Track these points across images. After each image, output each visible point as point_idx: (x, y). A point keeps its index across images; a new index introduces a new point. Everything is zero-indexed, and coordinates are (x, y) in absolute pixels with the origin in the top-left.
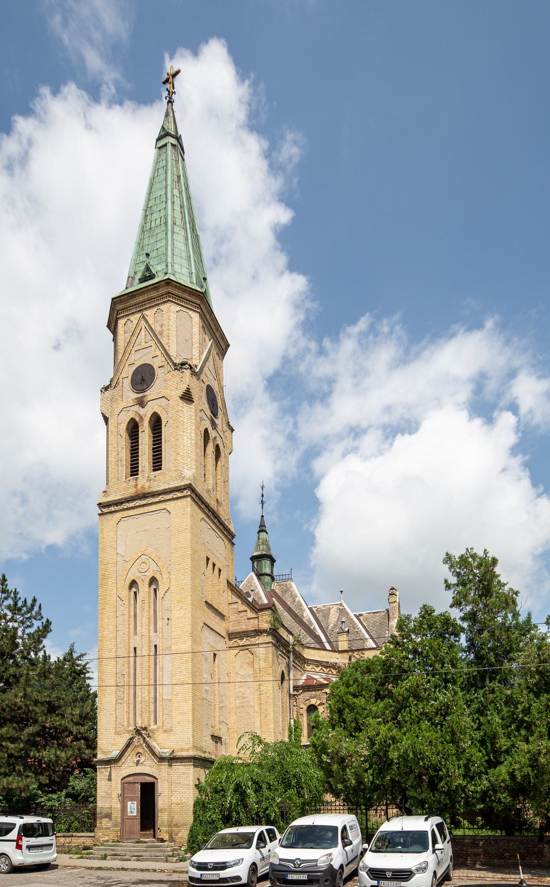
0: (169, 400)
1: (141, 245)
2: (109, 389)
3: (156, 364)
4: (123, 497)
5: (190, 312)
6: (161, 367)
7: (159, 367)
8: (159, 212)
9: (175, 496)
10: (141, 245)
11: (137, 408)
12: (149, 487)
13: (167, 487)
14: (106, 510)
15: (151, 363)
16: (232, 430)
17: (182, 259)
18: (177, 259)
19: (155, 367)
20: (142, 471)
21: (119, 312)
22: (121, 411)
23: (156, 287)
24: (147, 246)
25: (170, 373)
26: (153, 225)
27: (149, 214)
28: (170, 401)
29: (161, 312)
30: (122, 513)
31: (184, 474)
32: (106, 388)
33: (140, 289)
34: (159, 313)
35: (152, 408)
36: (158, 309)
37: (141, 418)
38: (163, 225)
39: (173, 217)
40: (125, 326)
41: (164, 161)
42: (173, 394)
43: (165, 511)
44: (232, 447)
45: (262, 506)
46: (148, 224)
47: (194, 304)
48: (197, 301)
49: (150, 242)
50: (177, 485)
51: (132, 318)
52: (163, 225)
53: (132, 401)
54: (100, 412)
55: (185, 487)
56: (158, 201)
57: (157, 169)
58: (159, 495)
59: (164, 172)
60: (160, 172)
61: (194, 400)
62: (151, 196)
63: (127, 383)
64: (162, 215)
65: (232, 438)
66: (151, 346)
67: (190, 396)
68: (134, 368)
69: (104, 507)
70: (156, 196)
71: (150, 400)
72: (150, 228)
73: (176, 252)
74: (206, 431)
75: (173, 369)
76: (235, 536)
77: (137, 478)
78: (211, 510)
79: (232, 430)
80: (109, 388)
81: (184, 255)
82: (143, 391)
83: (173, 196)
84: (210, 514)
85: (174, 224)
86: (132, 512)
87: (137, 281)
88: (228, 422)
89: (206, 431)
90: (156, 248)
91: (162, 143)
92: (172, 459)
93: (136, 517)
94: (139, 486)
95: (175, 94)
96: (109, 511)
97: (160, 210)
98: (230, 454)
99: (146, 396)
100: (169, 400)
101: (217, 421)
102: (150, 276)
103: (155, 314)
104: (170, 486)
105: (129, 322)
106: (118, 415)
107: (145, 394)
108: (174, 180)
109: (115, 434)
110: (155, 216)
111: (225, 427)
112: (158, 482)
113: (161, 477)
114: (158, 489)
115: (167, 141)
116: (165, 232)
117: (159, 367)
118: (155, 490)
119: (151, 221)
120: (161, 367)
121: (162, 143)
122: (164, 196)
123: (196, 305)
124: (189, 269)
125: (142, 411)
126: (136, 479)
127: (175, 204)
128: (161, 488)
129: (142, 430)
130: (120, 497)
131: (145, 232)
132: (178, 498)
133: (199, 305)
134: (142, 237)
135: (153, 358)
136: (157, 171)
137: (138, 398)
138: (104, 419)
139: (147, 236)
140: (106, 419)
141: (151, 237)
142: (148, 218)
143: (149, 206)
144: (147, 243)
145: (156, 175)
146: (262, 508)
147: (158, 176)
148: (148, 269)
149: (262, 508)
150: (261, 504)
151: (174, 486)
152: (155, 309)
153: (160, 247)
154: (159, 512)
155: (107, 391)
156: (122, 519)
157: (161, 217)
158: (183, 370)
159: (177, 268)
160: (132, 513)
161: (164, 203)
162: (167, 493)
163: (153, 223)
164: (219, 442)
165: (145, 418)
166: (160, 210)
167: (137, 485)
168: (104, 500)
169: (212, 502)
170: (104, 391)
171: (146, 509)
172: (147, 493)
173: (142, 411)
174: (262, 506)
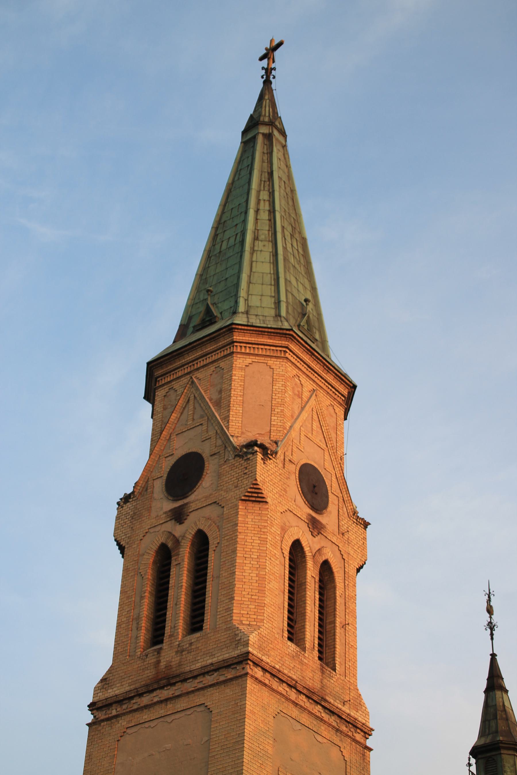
0: (223, 507)
1: (204, 277)
2: (130, 500)
3: (205, 450)
4: (132, 687)
5: (271, 362)
6: (215, 454)
7: (211, 456)
8: (234, 228)
9: (222, 678)
10: (204, 277)
11: (170, 526)
12: (180, 665)
13: (210, 661)
14: (102, 715)
15: (200, 451)
16: (366, 525)
17: (264, 286)
18: (256, 289)
19: (206, 455)
20: (171, 636)
21: (158, 379)
22: (146, 533)
23: (214, 338)
24: (212, 278)
25: (227, 462)
26: (224, 246)
27: (221, 231)
28: (225, 509)
29: (222, 371)
30: (128, 717)
31: (240, 635)
32: (126, 499)
33: (190, 344)
34: (217, 373)
35: (195, 523)
36: (216, 368)
37: (177, 542)
38: (237, 246)
39: (256, 231)
40: (166, 399)
41: (250, 158)
42: (230, 497)
43: (202, 708)
44: (364, 555)
45: (492, 635)
46: (218, 247)
47: (278, 348)
48: (283, 342)
49: (217, 271)
50: (227, 656)
51: (176, 385)
52: (237, 246)
53: (164, 515)
54: (113, 538)
55: (240, 660)
56: (235, 212)
57: (239, 170)
58: (195, 677)
59: (248, 172)
60: (243, 173)
61: (268, 500)
62: (226, 207)
63: (159, 486)
64: (239, 231)
65: (365, 539)
66: (202, 424)
67: (260, 495)
68: (172, 461)
69: (99, 709)
70: (233, 206)
71: (193, 511)
72: (218, 251)
73: (256, 278)
74: (297, 546)
75: (233, 456)
76: (372, 730)
77: (161, 649)
78: (305, 691)
79: (366, 525)
80: (130, 498)
81: (268, 279)
82: (184, 496)
83: (258, 201)
84: (302, 700)
85: (256, 238)
86: (145, 716)
87: (191, 329)
88: (355, 513)
89: (297, 546)
90: (224, 278)
91: (249, 136)
92: (221, 609)
93: (152, 724)
94: (163, 664)
95: (275, 70)
96: (107, 716)
97: (236, 225)
98: (358, 571)
99: (186, 504)
100: (223, 507)
101: (323, 519)
102: (210, 320)
103: (211, 375)
104: (215, 660)
105: (172, 392)
106: (141, 540)
107: (185, 501)
108: (263, 179)
109: (133, 574)
110: (228, 234)
111: (346, 523)
112: (195, 653)
113: (200, 645)
114: (193, 667)
115: (257, 132)
116: (239, 254)
117: (211, 456)
118: (188, 669)
119: (223, 241)
120: (215, 454)
121: (249, 136)
122: (244, 204)
123: (281, 349)
124: (274, 297)
125: (178, 530)
126: (159, 651)
127: (261, 212)
128: (199, 665)
129: (177, 563)
130: (128, 689)
131: (212, 258)
132: (225, 682)
133: (287, 348)
134: (207, 266)
135: (203, 441)
136: (238, 172)
137: (175, 508)
138: (119, 549)
139: (214, 263)
140: (122, 549)
141: (219, 265)
142: (219, 238)
143: (222, 221)
144: (212, 273)
145: (236, 179)
146: (492, 639)
147: (238, 179)
148: (208, 311)
149: (492, 639)
150: (489, 631)
151: (221, 658)
152: (212, 368)
153: (230, 276)
154: (192, 710)
155: (128, 504)
156: (128, 731)
157: (237, 234)
158: (249, 456)
159: (254, 301)
160: (146, 717)
161: (243, 214)
162: (208, 673)
163: (225, 244)
164: (330, 555)
165: (183, 541)
166: (236, 225)
167: (159, 662)
168: (102, 696)
169: (309, 674)
170: (122, 503)
171: (170, 707)
172: (173, 677)
173: (178, 530)
174: (492, 635)
